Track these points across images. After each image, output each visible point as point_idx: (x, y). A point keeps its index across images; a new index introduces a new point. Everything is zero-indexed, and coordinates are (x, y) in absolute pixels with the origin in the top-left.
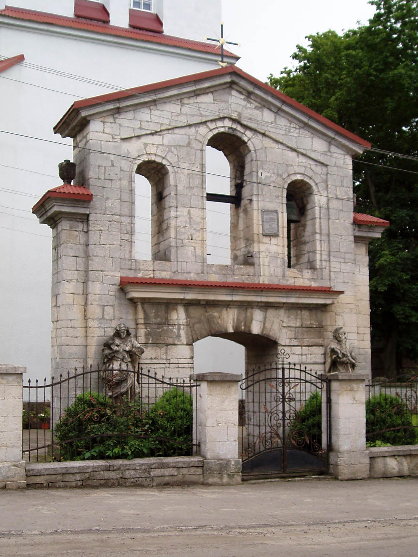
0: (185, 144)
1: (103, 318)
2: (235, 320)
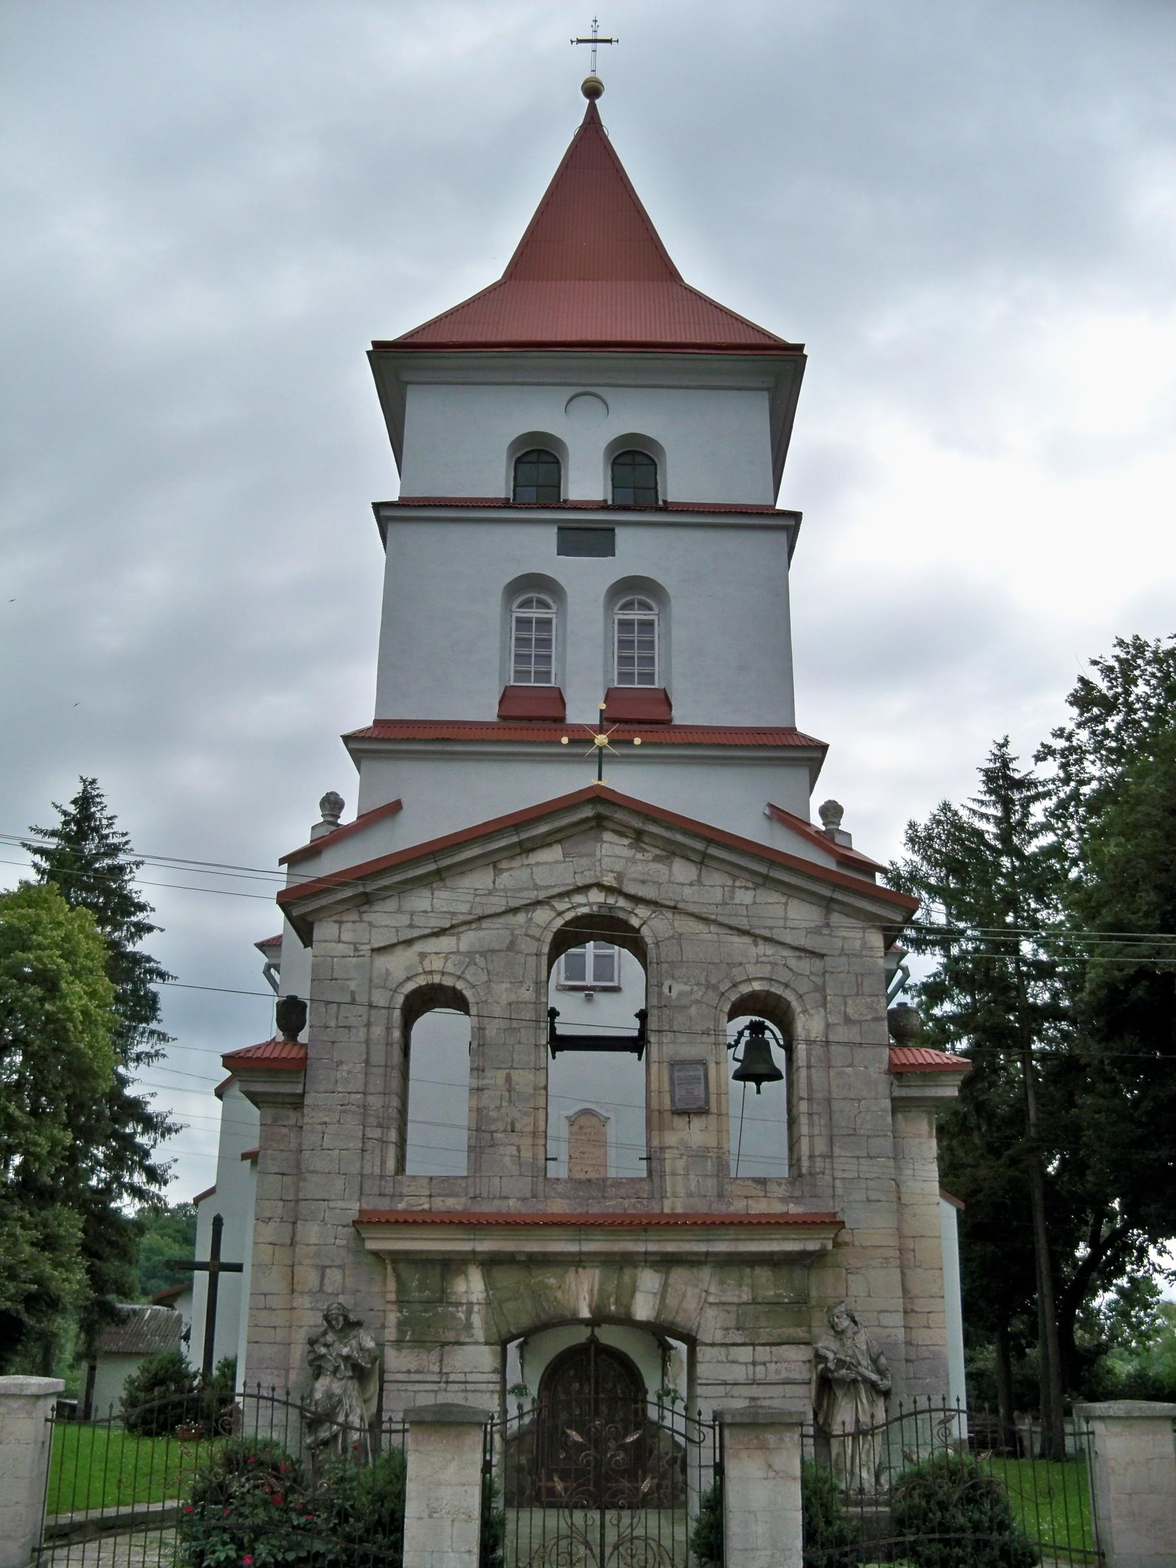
0: (504, 946)
1: (321, 1290)
2: (595, 1292)
